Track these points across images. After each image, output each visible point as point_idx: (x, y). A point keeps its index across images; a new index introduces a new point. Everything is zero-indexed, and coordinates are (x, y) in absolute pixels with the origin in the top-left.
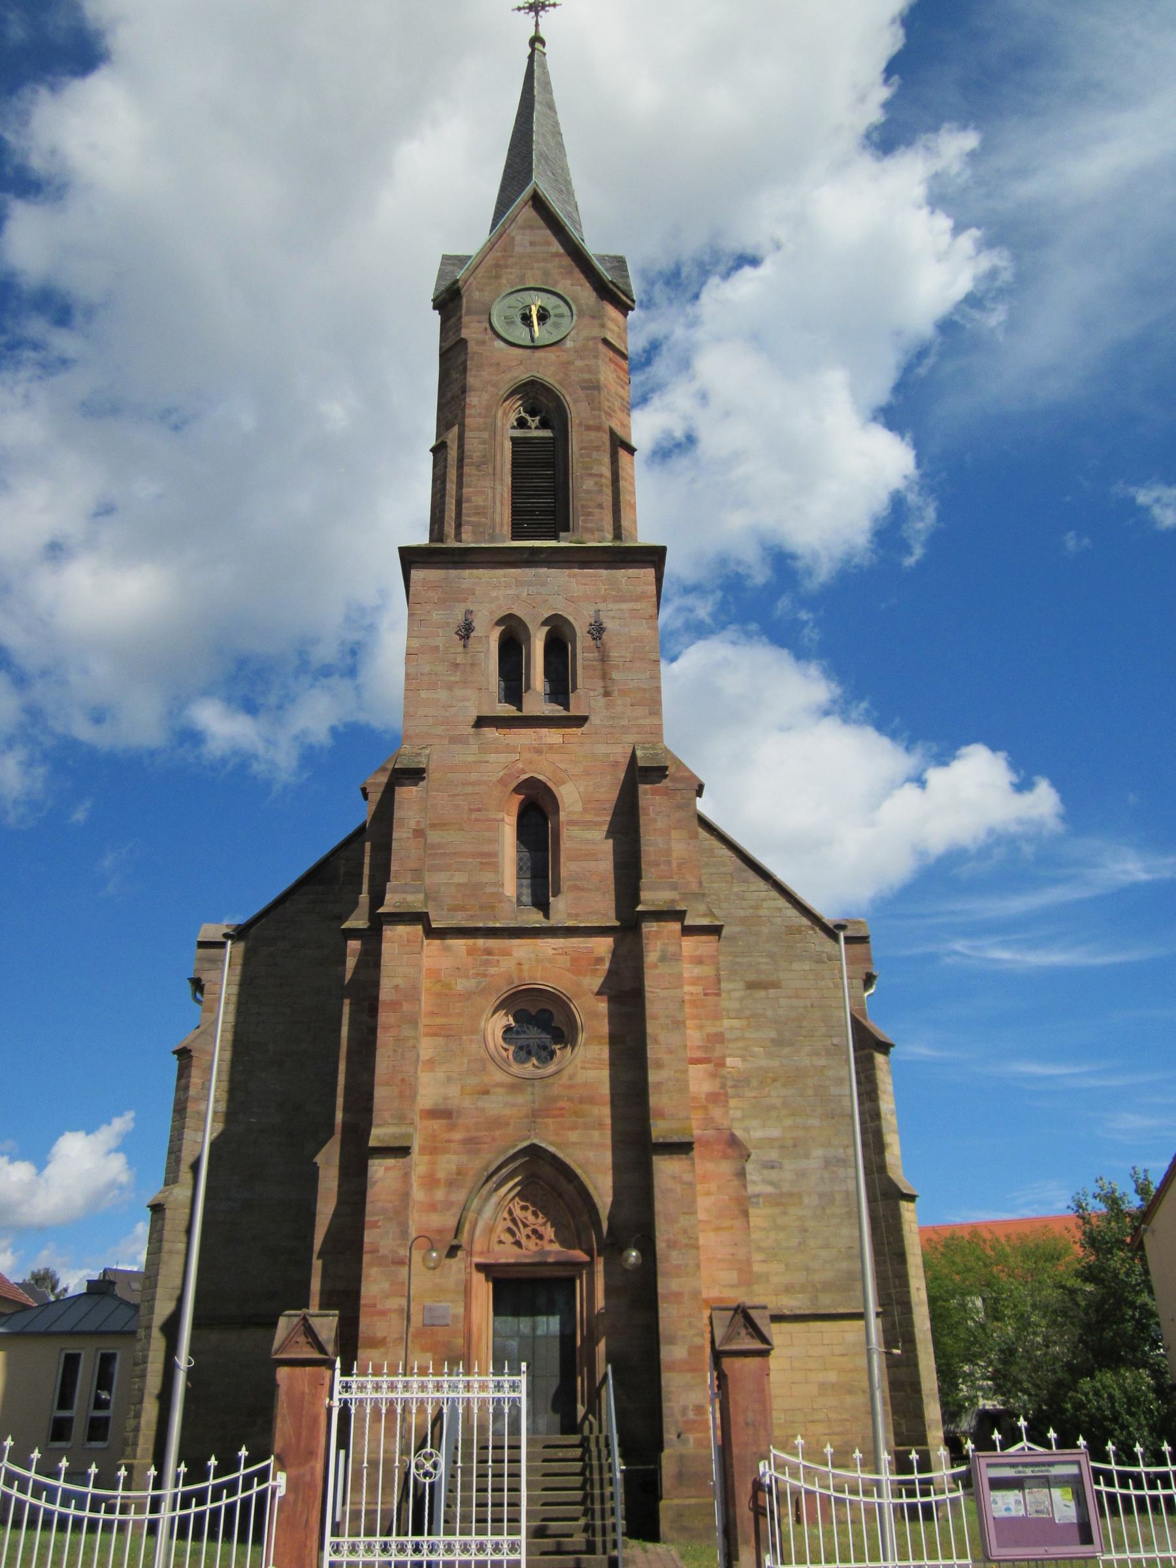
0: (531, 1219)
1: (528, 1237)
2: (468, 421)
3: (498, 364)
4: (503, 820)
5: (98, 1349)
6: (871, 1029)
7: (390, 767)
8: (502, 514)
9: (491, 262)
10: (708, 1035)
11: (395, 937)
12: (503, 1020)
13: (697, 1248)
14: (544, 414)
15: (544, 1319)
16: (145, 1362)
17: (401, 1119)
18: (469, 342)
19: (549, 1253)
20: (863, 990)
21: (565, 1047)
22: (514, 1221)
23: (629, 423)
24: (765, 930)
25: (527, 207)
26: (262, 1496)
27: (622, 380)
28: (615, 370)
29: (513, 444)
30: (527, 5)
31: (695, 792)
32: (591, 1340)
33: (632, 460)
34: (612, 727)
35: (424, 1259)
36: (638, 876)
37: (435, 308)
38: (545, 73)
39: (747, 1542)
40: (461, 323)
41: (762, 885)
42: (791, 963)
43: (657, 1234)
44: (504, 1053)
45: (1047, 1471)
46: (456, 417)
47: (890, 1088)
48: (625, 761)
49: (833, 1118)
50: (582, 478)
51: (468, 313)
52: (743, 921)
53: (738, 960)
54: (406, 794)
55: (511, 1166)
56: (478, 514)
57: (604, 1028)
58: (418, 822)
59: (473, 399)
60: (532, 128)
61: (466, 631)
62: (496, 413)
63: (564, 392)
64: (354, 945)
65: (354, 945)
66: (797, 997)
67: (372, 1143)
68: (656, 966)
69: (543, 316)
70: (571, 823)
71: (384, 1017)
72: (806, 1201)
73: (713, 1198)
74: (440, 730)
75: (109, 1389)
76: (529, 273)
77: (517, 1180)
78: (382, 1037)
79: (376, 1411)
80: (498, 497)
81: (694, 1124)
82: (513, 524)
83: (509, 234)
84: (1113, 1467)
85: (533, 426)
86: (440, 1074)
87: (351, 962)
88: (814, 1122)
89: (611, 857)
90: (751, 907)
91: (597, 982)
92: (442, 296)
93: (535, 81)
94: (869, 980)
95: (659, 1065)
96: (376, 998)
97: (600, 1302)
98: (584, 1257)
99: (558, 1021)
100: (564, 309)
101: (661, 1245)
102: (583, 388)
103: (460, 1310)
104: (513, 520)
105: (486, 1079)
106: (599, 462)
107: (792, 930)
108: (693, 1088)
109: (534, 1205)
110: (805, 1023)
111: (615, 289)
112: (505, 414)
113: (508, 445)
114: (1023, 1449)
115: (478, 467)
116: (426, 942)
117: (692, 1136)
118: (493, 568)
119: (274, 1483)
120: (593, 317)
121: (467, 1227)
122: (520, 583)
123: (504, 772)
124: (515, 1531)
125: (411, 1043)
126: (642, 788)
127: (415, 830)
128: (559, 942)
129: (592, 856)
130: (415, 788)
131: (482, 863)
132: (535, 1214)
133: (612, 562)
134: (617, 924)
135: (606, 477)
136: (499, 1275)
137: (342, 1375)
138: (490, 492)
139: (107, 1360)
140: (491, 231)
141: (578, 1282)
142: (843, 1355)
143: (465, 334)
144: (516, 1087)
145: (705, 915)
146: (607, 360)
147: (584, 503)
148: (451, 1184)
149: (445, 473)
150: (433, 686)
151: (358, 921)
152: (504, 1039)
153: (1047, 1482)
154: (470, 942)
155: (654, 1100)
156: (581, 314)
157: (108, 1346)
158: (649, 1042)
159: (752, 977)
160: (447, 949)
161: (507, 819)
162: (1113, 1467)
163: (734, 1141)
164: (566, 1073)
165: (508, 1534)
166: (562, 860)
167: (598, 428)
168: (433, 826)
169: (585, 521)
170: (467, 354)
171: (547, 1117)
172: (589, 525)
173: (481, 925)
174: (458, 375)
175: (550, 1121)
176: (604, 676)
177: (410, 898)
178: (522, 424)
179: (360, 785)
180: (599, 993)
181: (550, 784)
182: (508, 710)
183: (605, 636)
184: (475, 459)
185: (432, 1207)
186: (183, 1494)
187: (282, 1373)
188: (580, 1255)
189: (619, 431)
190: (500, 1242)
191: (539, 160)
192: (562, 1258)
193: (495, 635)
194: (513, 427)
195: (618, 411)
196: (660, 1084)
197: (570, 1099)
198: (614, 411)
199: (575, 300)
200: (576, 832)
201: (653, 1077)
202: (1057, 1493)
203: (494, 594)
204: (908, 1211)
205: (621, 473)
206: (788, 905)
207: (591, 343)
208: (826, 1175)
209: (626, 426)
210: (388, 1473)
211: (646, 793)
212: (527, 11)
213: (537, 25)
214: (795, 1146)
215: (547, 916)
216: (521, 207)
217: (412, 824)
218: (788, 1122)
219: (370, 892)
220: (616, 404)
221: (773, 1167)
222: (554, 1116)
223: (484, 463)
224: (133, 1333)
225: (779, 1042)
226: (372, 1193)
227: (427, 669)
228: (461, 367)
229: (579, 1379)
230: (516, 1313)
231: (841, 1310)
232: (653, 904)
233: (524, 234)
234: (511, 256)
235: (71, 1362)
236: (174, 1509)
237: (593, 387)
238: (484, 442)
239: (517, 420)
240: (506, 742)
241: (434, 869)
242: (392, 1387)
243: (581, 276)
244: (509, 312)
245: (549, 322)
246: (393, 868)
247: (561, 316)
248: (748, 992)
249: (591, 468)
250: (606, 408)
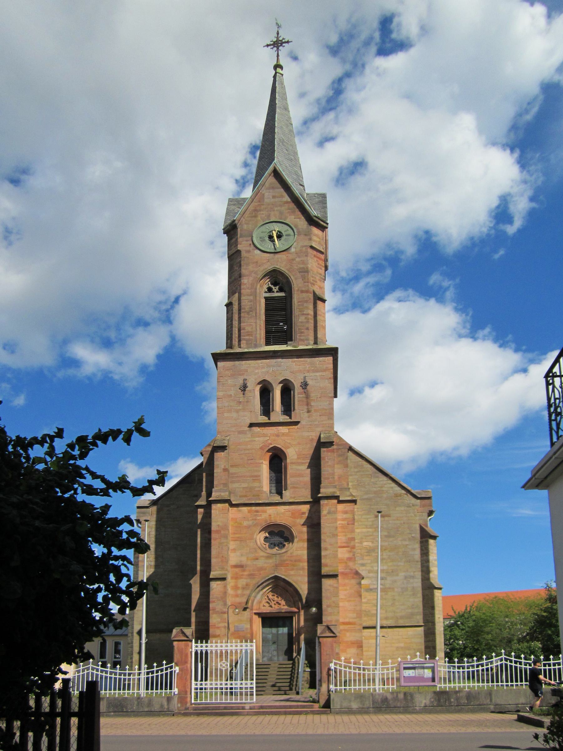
0: (276, 598)
1: (275, 604)
2: (242, 291)
3: (257, 262)
4: (262, 463)
5: (113, 640)
6: (429, 531)
7: (212, 444)
8: (260, 334)
9: (253, 208)
11: (216, 509)
12: (265, 534)
13: (339, 607)
14: (280, 285)
15: (282, 629)
16: (132, 643)
17: (223, 569)
18: (242, 252)
19: (283, 609)
21: (289, 543)
22: (269, 599)
23: (324, 286)
24: (385, 495)
25: (271, 177)
26: (171, 672)
27: (321, 265)
28: (317, 261)
31: (347, 450)
32: (299, 634)
33: (325, 305)
34: (310, 425)
35: (233, 612)
36: (320, 483)
37: (224, 233)
38: (283, 88)
39: (325, 682)
40: (237, 242)
41: (385, 478)
42: (395, 507)
43: (323, 603)
44: (264, 546)
46: (237, 289)
47: (435, 552)
48: (316, 439)
49: (410, 562)
50: (299, 316)
51: (241, 237)
52: (375, 492)
53: (372, 507)
54: (218, 456)
55: (270, 581)
56: (248, 335)
57: (305, 537)
58: (225, 466)
59: (245, 280)
60: (275, 125)
61: (244, 388)
62: (257, 286)
63: (290, 274)
64: (201, 510)
65: (201, 510)
66: (398, 520)
67: (211, 577)
68: (326, 516)
69: (279, 236)
70: (292, 463)
71: (213, 536)
72: (396, 590)
74: (233, 429)
75: (119, 654)
76: (272, 213)
77: (270, 587)
78: (213, 542)
80: (258, 326)
81: (339, 568)
82: (266, 338)
83: (261, 193)
85: (275, 291)
86: (238, 553)
87: (200, 517)
88: (402, 564)
89: (309, 476)
90: (379, 487)
91: (302, 521)
92: (228, 227)
93: (277, 94)
94: (431, 513)
95: (326, 549)
96: (211, 528)
97: (302, 623)
98: (296, 610)
99: (286, 534)
100: (291, 232)
101: (324, 606)
102: (300, 272)
103: (249, 626)
104: (266, 336)
105: (257, 555)
106: (307, 308)
107: (396, 495)
108: (340, 556)
109: (277, 594)
110: (400, 529)
111: (317, 219)
112: (261, 286)
113: (263, 301)
115: (248, 313)
116: (230, 509)
117: (338, 572)
118: (256, 360)
120: (306, 235)
121: (250, 602)
122: (269, 366)
125: (225, 544)
126: (322, 450)
127: (223, 469)
128: (287, 507)
129: (301, 475)
130: (223, 453)
132: (277, 597)
133: (312, 355)
134: (311, 500)
135: (311, 315)
136: (264, 616)
138: (254, 324)
139: (117, 644)
140: (253, 191)
141: (294, 618)
143: (240, 247)
144: (269, 557)
145: (349, 496)
146: (313, 256)
147: (300, 327)
148: (243, 588)
149: (232, 317)
150: (230, 411)
151: (202, 502)
152: (265, 541)
153: (424, 668)
154: (249, 508)
155: (323, 561)
156: (299, 234)
157: (117, 639)
158: (322, 542)
160: (240, 511)
161: (264, 462)
163: (357, 573)
164: (289, 552)
166: (288, 477)
167: (307, 292)
168: (232, 466)
169: (300, 336)
170: (241, 258)
173: (253, 502)
174: (237, 268)
176: (308, 404)
177: (222, 494)
178: (270, 290)
179: (200, 451)
180: (303, 525)
181: (283, 449)
182: (264, 419)
183: (308, 387)
184: (247, 310)
185: (237, 596)
186: (147, 672)
187: (175, 643)
188: (295, 610)
189: (318, 292)
190: (264, 606)
191: (279, 144)
192: (288, 610)
193: (258, 388)
194: (266, 292)
195: (318, 282)
196: (326, 555)
198: (316, 282)
199: (296, 226)
200: (294, 467)
201: (323, 553)
202: (426, 671)
203: (257, 371)
204: (437, 593)
205: (318, 313)
206: (396, 486)
207: (304, 249)
209: (322, 288)
211: (324, 452)
212: (272, 47)
213: (278, 56)
214: (392, 572)
215: (281, 498)
216: (268, 179)
217: (223, 467)
218: (390, 564)
219: (206, 491)
220: (317, 278)
222: (284, 566)
223: (251, 311)
224: (127, 635)
225: (388, 536)
226: (212, 593)
227: (227, 404)
228: (239, 264)
229: (294, 646)
230: (271, 627)
231: (407, 625)
232: (325, 494)
233: (269, 192)
234: (263, 205)
237: (305, 271)
238: (251, 301)
239: (267, 288)
240: (263, 432)
241: (233, 482)
243: (299, 213)
244: (262, 235)
245: (283, 238)
246: (215, 483)
247: (288, 235)
249: (303, 311)
250: (312, 281)
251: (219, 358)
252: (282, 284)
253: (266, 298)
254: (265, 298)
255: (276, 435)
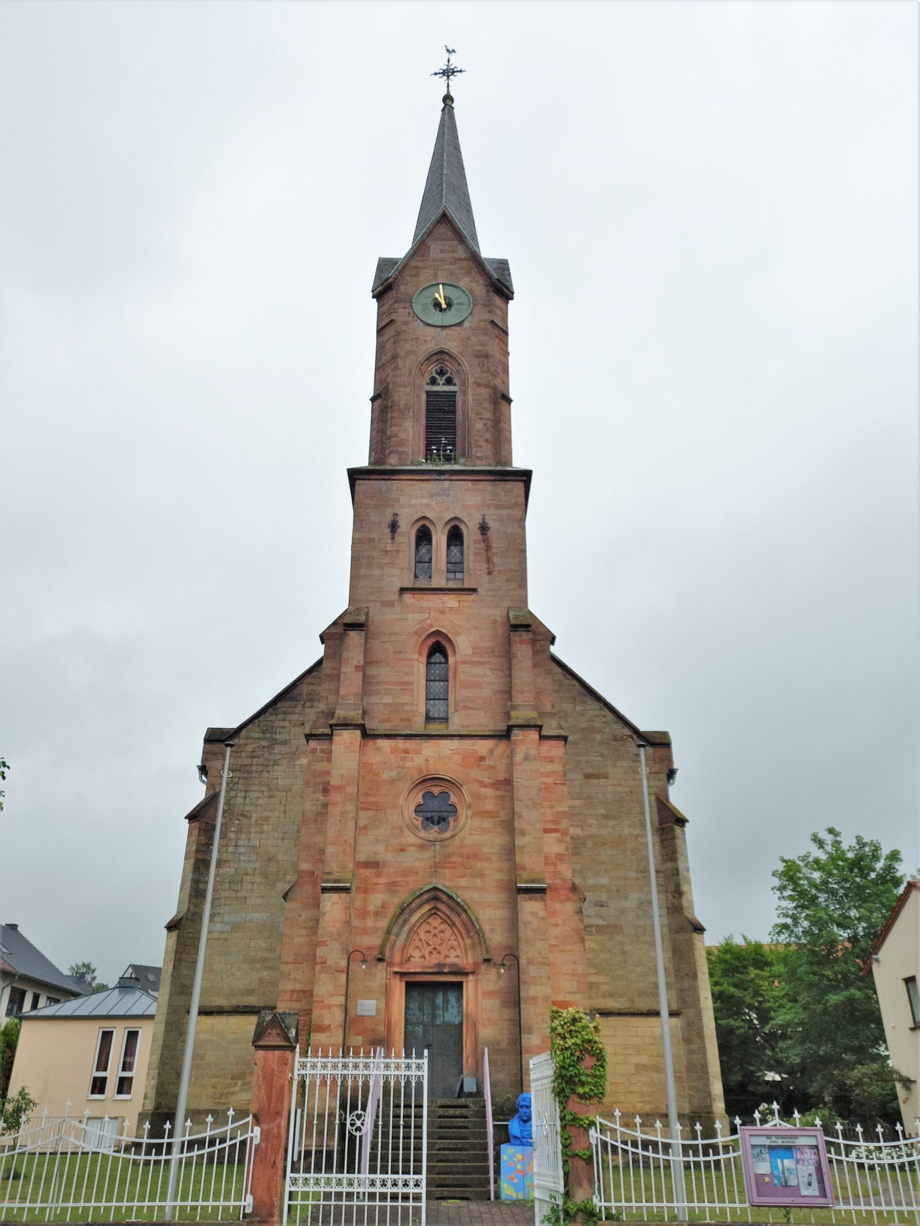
10: (557, 813)
20: (666, 782)
29: (427, 396)
30: (441, 71)
37: (373, 297)
41: (596, 705)
45: (793, 1142)
61: (394, 526)
66: (620, 785)
72: (626, 931)
73: (559, 928)
79: (324, 1083)
84: (841, 1141)
85: (441, 383)
101: (523, 962)
105: (403, 841)
113: (424, 397)
114: (775, 1125)
119: (252, 1135)
123: (419, 626)
124: (418, 1171)
127: (356, 666)
128: (454, 744)
131: (402, 689)
137: (300, 1057)
142: (652, 1044)
146: (494, 336)
148: (377, 914)
157: (133, 1025)
159: (589, 771)
162: (841, 1141)
163: (574, 888)
164: (458, 838)
165: (414, 1174)
169: (476, 452)
171: (445, 868)
172: (480, 455)
175: (446, 871)
176: (489, 560)
178: (433, 381)
186: (189, 1141)
189: (501, 387)
194: (428, 384)
195: (501, 373)
196: (523, 847)
197: (461, 856)
198: (498, 374)
208: (640, 913)
210: (331, 1123)
212: (441, 75)
213: (448, 86)
214: (618, 891)
217: (355, 662)
221: (602, 906)
235: (107, 1036)
236: (182, 1152)
242: (324, 1066)
248: (586, 780)
249: (482, 414)
251: (359, 477)
252: (451, 374)
253: (429, 394)
254: (427, 392)
255: (440, 610)
